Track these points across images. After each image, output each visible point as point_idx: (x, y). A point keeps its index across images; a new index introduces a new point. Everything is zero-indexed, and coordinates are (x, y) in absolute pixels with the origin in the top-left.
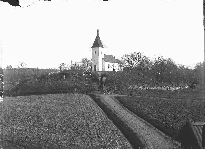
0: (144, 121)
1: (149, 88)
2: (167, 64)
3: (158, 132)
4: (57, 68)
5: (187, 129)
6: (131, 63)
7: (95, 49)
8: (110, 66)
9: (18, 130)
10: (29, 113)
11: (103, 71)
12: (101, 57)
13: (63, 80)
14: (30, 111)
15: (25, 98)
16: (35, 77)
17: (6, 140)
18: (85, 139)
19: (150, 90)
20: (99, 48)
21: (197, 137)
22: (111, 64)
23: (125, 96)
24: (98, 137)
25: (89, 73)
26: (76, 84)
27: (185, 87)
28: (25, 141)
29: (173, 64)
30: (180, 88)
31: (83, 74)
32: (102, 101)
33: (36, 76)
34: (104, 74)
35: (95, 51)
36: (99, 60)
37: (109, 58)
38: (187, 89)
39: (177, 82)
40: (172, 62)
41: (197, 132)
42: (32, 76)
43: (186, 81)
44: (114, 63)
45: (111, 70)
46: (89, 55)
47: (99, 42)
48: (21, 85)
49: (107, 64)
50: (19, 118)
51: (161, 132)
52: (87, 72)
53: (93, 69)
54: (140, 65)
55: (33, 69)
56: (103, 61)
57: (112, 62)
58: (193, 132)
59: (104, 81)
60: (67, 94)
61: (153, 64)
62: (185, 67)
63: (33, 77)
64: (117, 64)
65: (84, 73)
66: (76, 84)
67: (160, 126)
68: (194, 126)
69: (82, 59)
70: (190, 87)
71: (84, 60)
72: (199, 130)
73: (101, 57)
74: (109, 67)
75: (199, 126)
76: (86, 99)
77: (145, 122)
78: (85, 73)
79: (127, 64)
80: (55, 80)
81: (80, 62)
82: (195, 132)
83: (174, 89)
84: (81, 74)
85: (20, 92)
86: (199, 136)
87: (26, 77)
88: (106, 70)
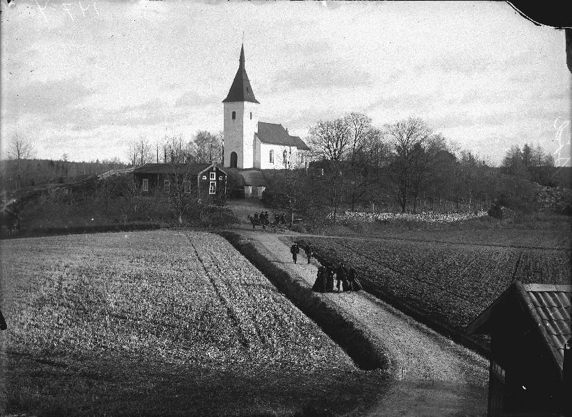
0: (377, 300)
1: (384, 216)
2: (431, 150)
3: (417, 327)
4: (126, 160)
5: (512, 301)
6: (335, 147)
7: (234, 106)
8: (274, 156)
9: (36, 326)
10: (60, 284)
11: (256, 168)
12: (250, 129)
13: (144, 194)
14: (61, 278)
15: (39, 244)
16: (61, 184)
17: (7, 352)
18: (226, 346)
19: (385, 222)
20: (246, 103)
21: (538, 318)
22: (278, 149)
23: (321, 237)
24: (263, 340)
25: (219, 173)
26: (184, 204)
27: (476, 213)
28: (63, 354)
29: (447, 152)
30: (465, 217)
31: (202, 177)
32: (261, 251)
33: (61, 181)
34: (267, 178)
35: (234, 113)
36: (245, 139)
37: (270, 133)
38: (482, 219)
39: (456, 201)
40: (444, 146)
41: (536, 306)
42: (51, 182)
43: (479, 197)
44: (287, 148)
45: (279, 165)
46: (215, 125)
47: (245, 89)
48: (18, 207)
49: (265, 148)
50: (34, 296)
51: (424, 327)
52: (211, 170)
53: (227, 164)
54: (357, 153)
55: (51, 163)
56: (255, 140)
57: (280, 144)
58: (526, 305)
59: (260, 195)
60: (159, 232)
61: (395, 151)
62: (389, 139)
63: (53, 185)
64: (294, 149)
65: (204, 174)
66: (184, 204)
67: (419, 312)
68: (528, 292)
69: (195, 134)
70: (490, 213)
71: (202, 138)
72: (541, 302)
73: (250, 129)
74: (272, 158)
75: (540, 292)
76: (213, 247)
77: (381, 302)
78: (207, 173)
79: (322, 150)
80: (121, 195)
81: (191, 143)
82: (531, 306)
83: (450, 218)
84: (194, 179)
85: (18, 227)
86: (541, 316)
87: (33, 184)
88: (266, 165)
